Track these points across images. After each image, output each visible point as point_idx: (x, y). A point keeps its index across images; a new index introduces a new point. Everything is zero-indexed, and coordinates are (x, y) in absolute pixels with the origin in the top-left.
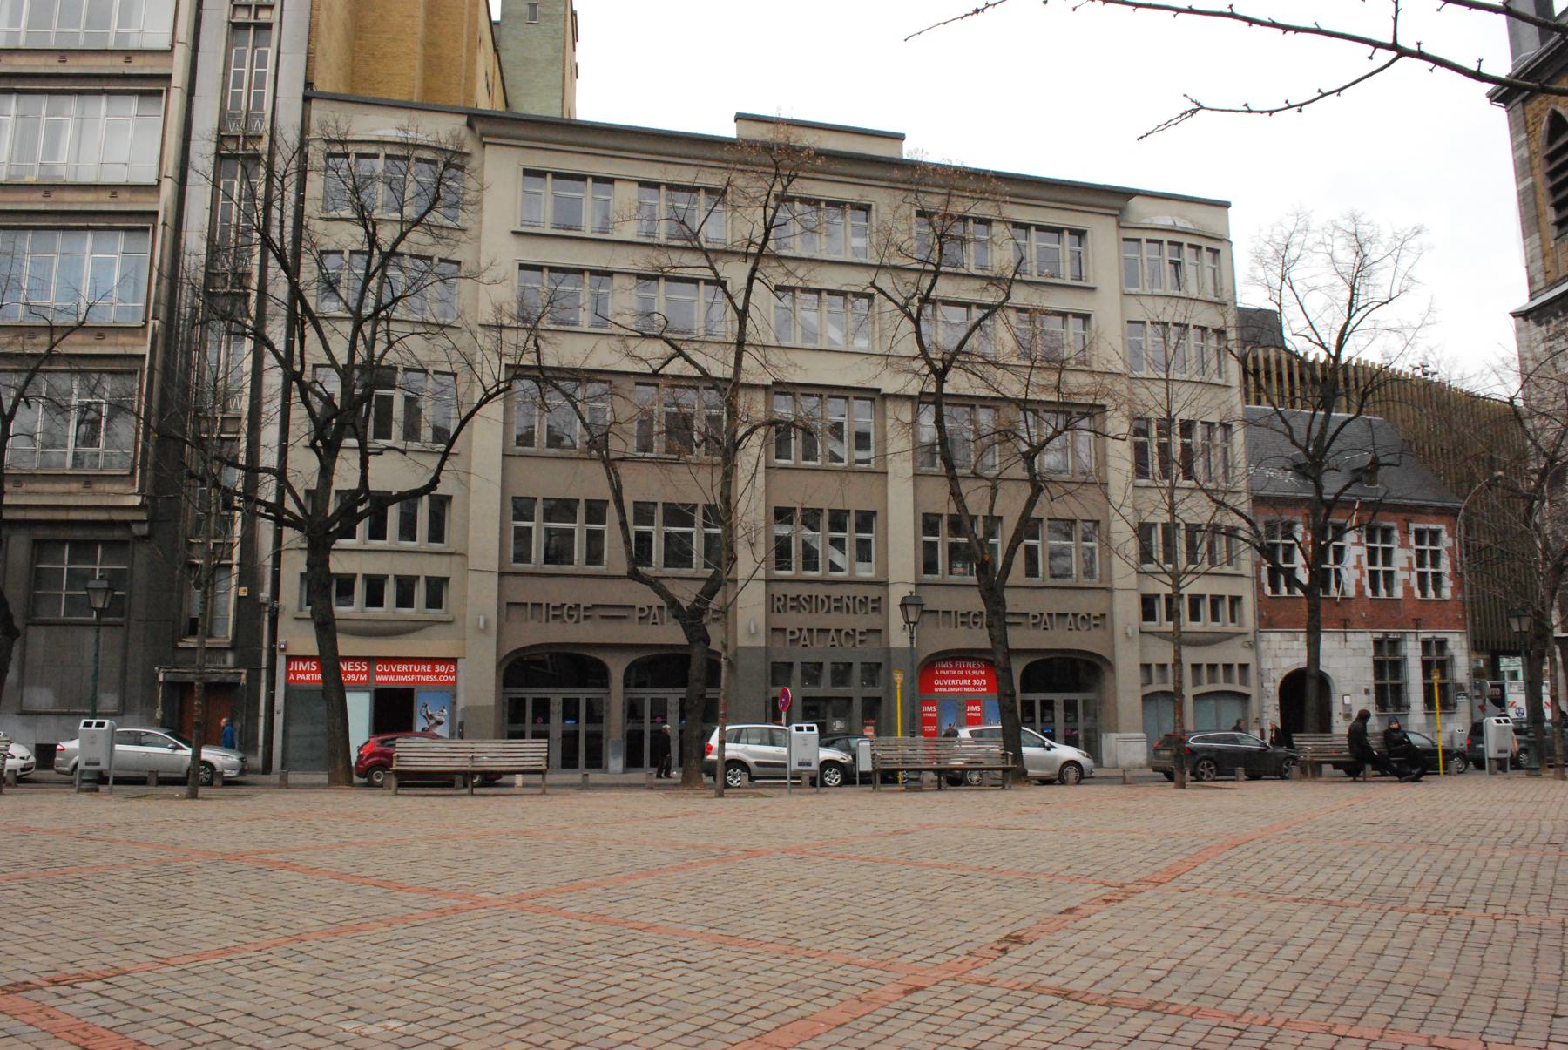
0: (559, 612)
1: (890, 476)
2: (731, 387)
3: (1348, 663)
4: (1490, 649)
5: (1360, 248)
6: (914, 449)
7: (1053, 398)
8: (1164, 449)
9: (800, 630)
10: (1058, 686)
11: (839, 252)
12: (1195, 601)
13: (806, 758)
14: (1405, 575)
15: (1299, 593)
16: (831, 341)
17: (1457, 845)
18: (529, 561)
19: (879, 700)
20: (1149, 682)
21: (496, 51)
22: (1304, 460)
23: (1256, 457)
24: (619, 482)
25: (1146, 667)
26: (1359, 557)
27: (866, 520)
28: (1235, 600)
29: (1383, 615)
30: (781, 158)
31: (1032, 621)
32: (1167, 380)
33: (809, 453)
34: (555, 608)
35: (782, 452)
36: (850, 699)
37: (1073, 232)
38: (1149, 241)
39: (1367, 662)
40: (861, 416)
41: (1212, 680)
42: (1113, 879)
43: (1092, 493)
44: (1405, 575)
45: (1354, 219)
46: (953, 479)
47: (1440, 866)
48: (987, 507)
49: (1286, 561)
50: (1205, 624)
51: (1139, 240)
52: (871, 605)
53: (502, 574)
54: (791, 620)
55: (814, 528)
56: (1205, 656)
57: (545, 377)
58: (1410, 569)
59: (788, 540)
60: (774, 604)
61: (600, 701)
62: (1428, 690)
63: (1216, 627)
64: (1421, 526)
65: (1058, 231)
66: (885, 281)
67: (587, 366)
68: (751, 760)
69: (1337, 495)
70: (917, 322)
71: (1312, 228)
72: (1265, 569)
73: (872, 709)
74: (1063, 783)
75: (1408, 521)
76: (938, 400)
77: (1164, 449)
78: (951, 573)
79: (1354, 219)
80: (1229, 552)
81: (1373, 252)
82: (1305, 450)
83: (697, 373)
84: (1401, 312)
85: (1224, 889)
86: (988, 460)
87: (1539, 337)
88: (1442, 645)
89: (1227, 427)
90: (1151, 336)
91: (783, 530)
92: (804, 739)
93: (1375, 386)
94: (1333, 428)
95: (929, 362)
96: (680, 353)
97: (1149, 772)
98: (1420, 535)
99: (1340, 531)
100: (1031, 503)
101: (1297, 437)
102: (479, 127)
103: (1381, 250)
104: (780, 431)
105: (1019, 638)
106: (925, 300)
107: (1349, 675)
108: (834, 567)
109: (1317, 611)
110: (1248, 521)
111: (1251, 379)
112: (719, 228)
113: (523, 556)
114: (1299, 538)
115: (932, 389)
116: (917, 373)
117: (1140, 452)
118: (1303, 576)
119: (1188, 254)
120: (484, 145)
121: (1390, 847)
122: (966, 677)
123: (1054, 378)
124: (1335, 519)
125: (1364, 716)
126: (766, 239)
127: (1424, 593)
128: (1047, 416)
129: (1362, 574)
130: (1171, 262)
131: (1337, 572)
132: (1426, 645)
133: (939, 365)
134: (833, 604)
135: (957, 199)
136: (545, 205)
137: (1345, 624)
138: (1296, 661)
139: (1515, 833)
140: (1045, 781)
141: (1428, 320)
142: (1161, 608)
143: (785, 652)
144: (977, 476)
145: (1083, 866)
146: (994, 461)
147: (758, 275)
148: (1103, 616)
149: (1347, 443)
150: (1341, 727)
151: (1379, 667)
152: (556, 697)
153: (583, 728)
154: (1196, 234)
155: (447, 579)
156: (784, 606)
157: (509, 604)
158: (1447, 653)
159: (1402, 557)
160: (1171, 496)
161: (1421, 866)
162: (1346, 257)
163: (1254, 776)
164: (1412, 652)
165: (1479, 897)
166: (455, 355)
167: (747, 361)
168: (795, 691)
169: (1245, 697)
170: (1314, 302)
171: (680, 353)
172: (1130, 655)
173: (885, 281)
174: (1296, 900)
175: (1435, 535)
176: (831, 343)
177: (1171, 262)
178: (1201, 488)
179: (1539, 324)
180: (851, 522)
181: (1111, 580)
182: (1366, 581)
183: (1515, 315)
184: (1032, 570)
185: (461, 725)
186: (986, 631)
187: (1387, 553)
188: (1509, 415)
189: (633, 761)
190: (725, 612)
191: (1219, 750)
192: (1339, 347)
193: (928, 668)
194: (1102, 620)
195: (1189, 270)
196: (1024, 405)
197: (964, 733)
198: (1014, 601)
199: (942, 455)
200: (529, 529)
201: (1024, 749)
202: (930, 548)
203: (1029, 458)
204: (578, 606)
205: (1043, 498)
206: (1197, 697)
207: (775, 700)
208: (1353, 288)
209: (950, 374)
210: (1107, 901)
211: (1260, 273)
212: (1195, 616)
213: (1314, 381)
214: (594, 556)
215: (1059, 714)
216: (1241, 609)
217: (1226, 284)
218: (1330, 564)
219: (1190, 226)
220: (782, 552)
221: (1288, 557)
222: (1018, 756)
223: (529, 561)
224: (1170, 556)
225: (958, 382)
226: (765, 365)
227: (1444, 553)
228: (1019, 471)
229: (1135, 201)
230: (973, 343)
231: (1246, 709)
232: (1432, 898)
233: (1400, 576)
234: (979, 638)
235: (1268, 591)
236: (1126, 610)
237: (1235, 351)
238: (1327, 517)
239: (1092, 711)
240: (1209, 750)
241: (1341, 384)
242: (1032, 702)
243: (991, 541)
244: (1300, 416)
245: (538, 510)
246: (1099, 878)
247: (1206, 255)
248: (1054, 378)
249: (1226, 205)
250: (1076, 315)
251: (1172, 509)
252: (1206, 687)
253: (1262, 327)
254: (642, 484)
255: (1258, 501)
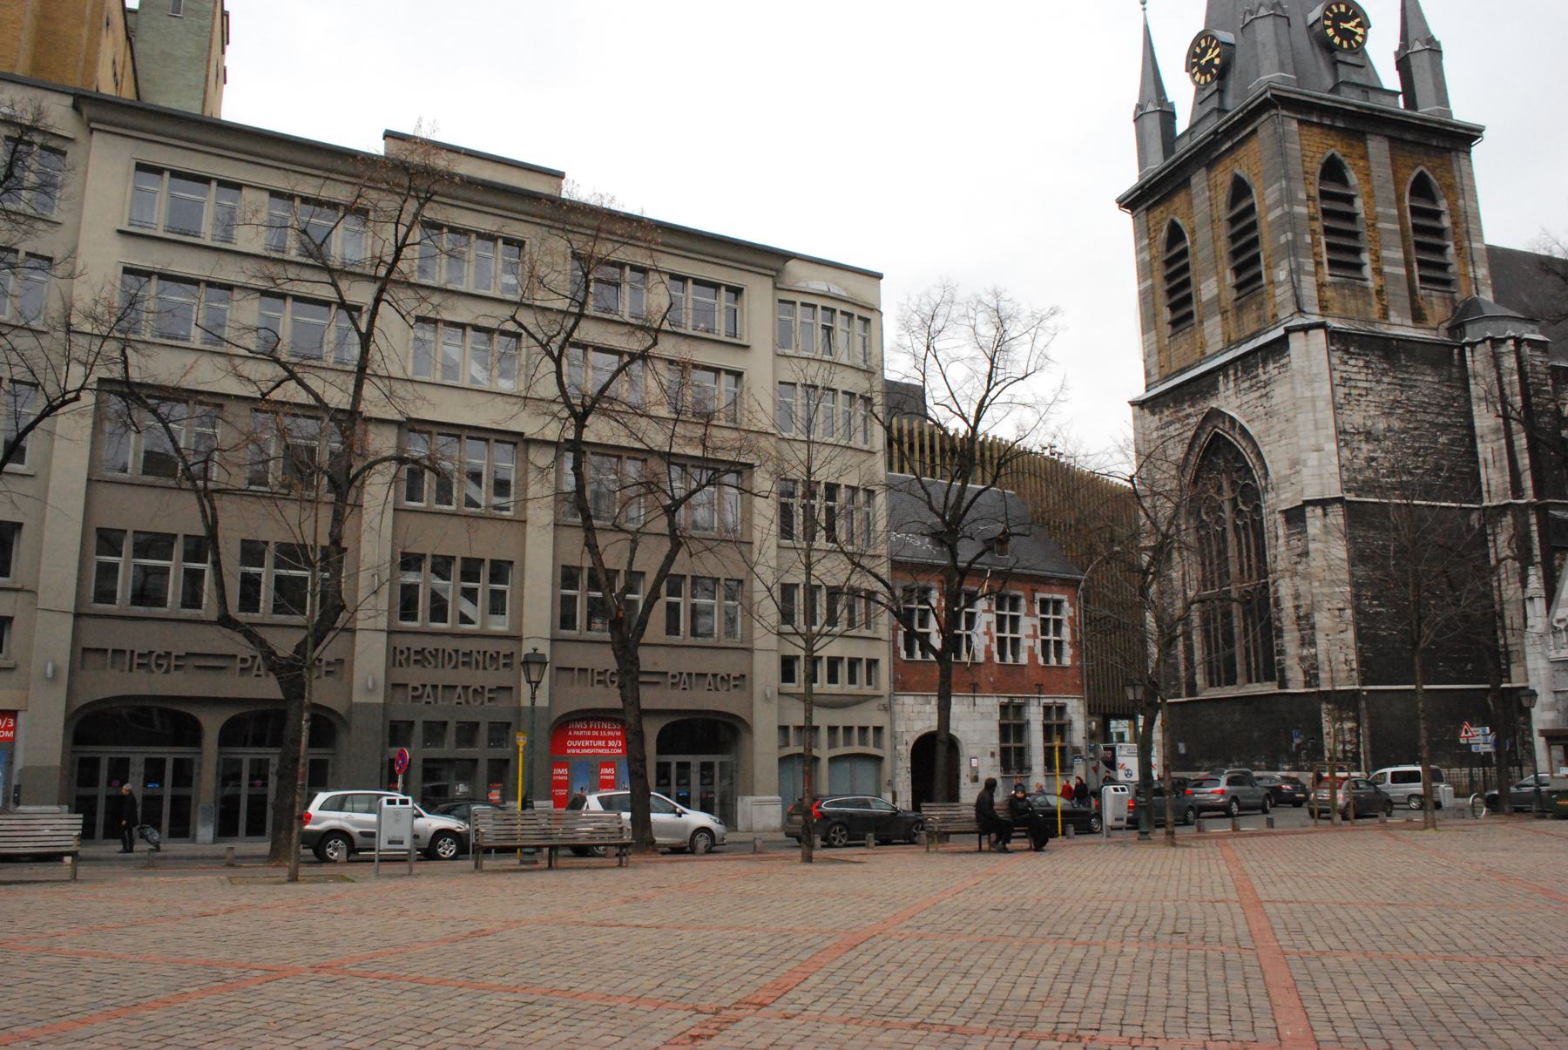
0: (146, 661)
1: (529, 528)
2: (351, 419)
3: (975, 725)
4: (1102, 713)
5: (1000, 324)
6: (556, 494)
7: (698, 453)
8: (809, 510)
9: (424, 686)
10: (699, 746)
11: (488, 288)
12: (834, 663)
13: (397, 835)
14: (1030, 642)
15: (932, 657)
16: (474, 380)
17: (1084, 938)
18: (164, 605)
19: (507, 761)
20: (787, 745)
21: (128, 39)
22: (940, 527)
23: (895, 525)
24: (214, 516)
25: (784, 729)
26: (989, 624)
27: (500, 570)
28: (872, 663)
29: (1010, 681)
30: (419, 179)
31: (671, 681)
32: (809, 442)
33: (444, 494)
34: (141, 655)
35: (413, 493)
36: (475, 762)
37: (730, 289)
38: (803, 304)
39: (993, 725)
40: (504, 461)
41: (848, 743)
42: (710, 1002)
43: (730, 552)
44: (1030, 642)
45: (997, 295)
46: (589, 530)
47: (1068, 970)
48: (625, 561)
49: (921, 626)
50: (842, 687)
51: (794, 303)
52: (502, 661)
53: (78, 616)
54: (414, 675)
55: (445, 577)
56: (840, 718)
57: (130, 392)
58: (1035, 636)
59: (415, 587)
60: (395, 657)
61: (191, 761)
62: (1048, 753)
63: (853, 689)
64: (1047, 596)
65: (716, 286)
66: (526, 318)
67: (184, 385)
68: (355, 830)
69: (970, 563)
70: (558, 362)
71: (957, 300)
72: (901, 633)
73: (500, 771)
74: (693, 852)
75: (1034, 591)
76: (577, 447)
77: (809, 510)
78: (589, 629)
79: (997, 295)
80: (868, 615)
81: (1013, 330)
82: (942, 517)
83: (312, 401)
84: (1038, 387)
85: (835, 1013)
86: (633, 512)
87: (1153, 426)
88: (1061, 709)
89: (870, 494)
90: (798, 400)
91: (410, 578)
92: (397, 813)
93: (1006, 461)
94: (968, 496)
95: (570, 406)
96: (292, 376)
97: (782, 836)
98: (1044, 604)
99: (972, 599)
100: (670, 559)
101: (934, 503)
102: (87, 111)
103: (1020, 327)
104: (413, 474)
105: (650, 698)
106: (568, 342)
107: (977, 738)
108: (465, 619)
109: (947, 675)
110: (886, 585)
111: (895, 446)
112: (349, 244)
113: (105, 594)
114: (934, 604)
115: (570, 435)
116: (555, 415)
117: (786, 512)
118: (936, 641)
119: (839, 322)
120: (92, 131)
121: (1017, 943)
122: (601, 738)
123: (700, 431)
124: (968, 586)
125: (991, 785)
126: (397, 259)
127: (1046, 660)
128: (691, 470)
129: (991, 639)
130: (824, 327)
131: (968, 637)
132: (1047, 709)
133: (579, 409)
134: (461, 659)
135: (612, 241)
136: (161, 202)
137: (974, 689)
138: (928, 723)
139: (1140, 921)
140: (676, 850)
141: (1061, 397)
142: (800, 670)
143: (404, 709)
144: (618, 529)
145: (678, 982)
146: (637, 513)
147: (385, 296)
148: (340, 661)
149: (979, 510)
150: (969, 793)
151: (1004, 731)
152: (138, 758)
153: (168, 791)
154: (848, 303)
155: (10, 619)
156: (408, 659)
157: (85, 650)
158: (1066, 718)
159: (1028, 625)
160: (808, 557)
161: (1051, 969)
162: (988, 332)
163: (884, 841)
164: (1035, 716)
165: (1113, 1014)
166: (15, 359)
167: (368, 390)
168: (415, 753)
169: (878, 760)
170: (957, 373)
171: (292, 376)
172: (768, 717)
173: (526, 318)
174: (915, 1027)
175: (1058, 603)
176: (456, 376)
177: (824, 327)
178: (842, 551)
179: (1153, 413)
180: (485, 573)
181: (751, 641)
182: (994, 647)
183: (1133, 404)
184: (672, 628)
185: (18, 788)
186: (618, 691)
187: (1015, 621)
188: (1125, 500)
189: (226, 829)
190: (340, 667)
191: (851, 815)
192: (978, 419)
193: (563, 726)
194: (742, 681)
195: (840, 338)
196: (669, 458)
197: (593, 802)
198: (648, 659)
199: (580, 508)
200: (115, 566)
201: (653, 816)
202: (567, 604)
203: (671, 511)
204: (169, 654)
205: (682, 556)
206: (832, 760)
207: (392, 761)
208: (992, 361)
209: (590, 420)
210: (694, 1038)
211: (907, 341)
212: (833, 678)
213: (953, 450)
214: (192, 598)
215: (695, 778)
216: (877, 673)
217: (875, 351)
218: (962, 630)
219: (844, 294)
220: (408, 605)
221: (924, 622)
222: (647, 822)
223: (164, 605)
224: (811, 619)
225: (599, 430)
226: (390, 397)
227: (1066, 622)
228: (662, 525)
229: (791, 264)
230: (621, 389)
231: (879, 770)
232: (1064, 1017)
233: (1025, 643)
234: (610, 698)
235: (903, 654)
236: (766, 670)
237: (881, 416)
238: (960, 583)
239: (729, 772)
240: (842, 814)
241: (978, 454)
242: (668, 764)
243: (629, 596)
244: (939, 485)
245: (127, 546)
246: (691, 1000)
247: (857, 323)
248: (700, 431)
249: (879, 276)
250: (728, 372)
251: (809, 567)
252: (841, 750)
253: (907, 399)
254: (239, 523)
255: (896, 566)
